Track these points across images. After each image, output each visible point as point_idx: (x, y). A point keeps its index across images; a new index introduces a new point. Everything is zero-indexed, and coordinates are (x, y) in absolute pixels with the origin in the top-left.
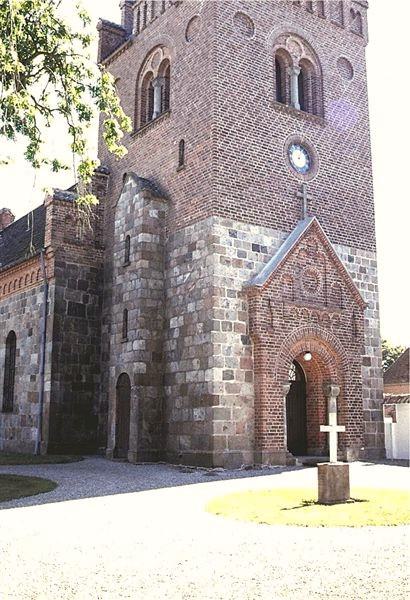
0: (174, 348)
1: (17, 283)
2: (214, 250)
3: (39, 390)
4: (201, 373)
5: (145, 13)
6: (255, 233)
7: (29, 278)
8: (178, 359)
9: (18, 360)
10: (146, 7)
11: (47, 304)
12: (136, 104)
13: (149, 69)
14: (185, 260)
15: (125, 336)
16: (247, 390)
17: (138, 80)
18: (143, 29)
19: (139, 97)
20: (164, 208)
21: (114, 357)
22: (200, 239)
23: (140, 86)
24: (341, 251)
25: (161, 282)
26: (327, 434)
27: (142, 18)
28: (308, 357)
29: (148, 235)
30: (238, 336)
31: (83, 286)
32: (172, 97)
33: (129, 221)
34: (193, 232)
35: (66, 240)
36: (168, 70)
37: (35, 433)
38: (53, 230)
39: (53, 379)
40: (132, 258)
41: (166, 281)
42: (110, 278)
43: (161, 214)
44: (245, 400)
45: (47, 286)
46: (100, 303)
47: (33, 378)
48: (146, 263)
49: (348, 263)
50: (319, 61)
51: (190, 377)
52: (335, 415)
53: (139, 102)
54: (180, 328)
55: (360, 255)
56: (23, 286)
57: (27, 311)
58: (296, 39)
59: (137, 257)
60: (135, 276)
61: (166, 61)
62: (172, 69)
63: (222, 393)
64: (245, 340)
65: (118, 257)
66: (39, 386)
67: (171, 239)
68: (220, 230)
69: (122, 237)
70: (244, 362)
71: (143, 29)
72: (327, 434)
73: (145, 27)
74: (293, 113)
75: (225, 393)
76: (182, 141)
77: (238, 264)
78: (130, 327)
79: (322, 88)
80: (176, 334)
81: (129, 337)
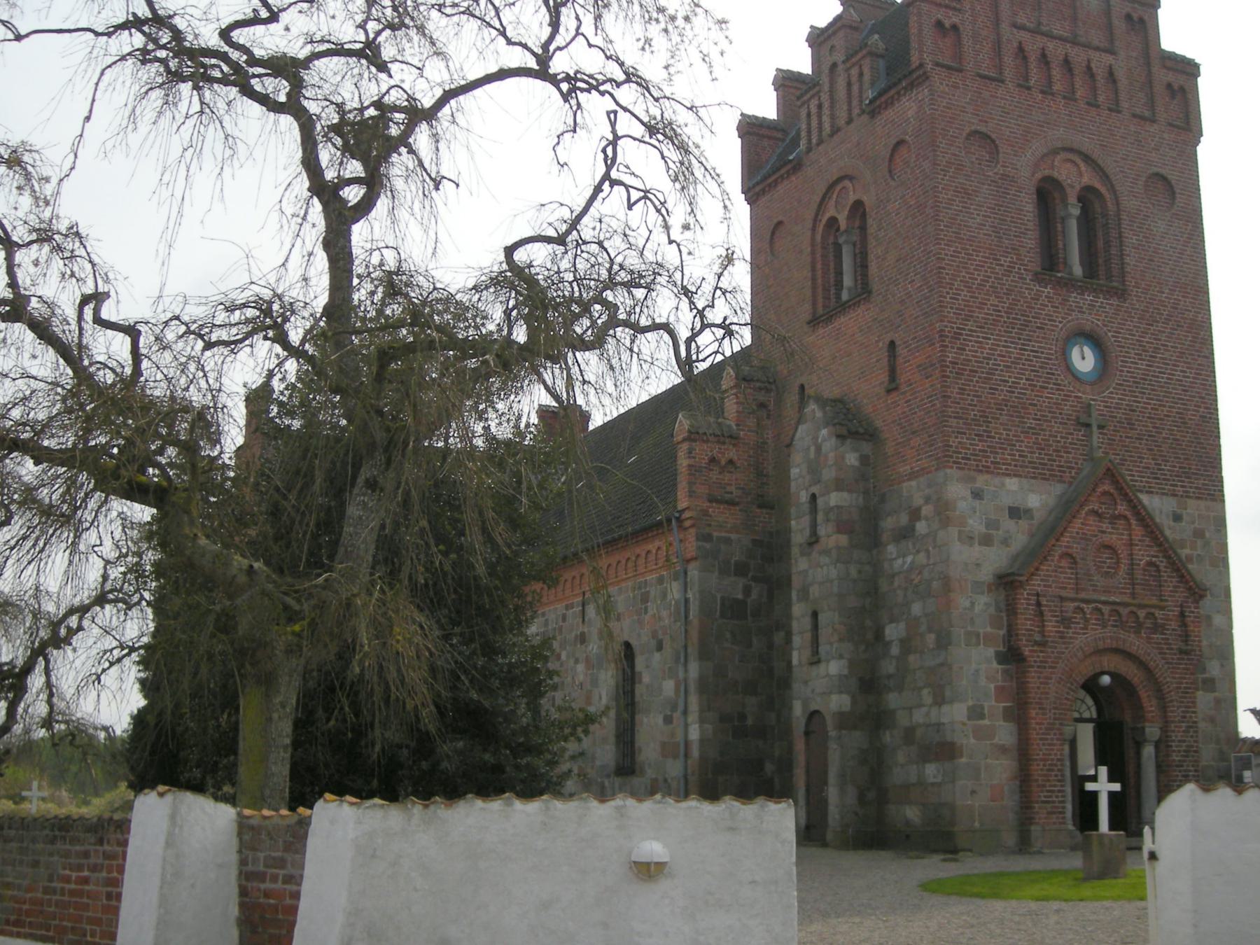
1: (630, 564)
2: (946, 522)
4: (934, 711)
5: (820, 116)
6: (1012, 488)
7: (652, 557)
8: (900, 688)
9: (639, 690)
10: (820, 106)
11: (687, 601)
12: (813, 269)
13: (831, 212)
14: (905, 534)
15: (816, 652)
16: (1005, 734)
17: (814, 229)
18: (818, 145)
19: (818, 256)
20: (867, 448)
21: (796, 686)
23: (819, 238)
24: (1157, 505)
26: (1095, 795)
27: (814, 123)
28: (1106, 680)
29: (845, 495)
30: (990, 652)
31: (741, 570)
32: (873, 269)
33: (814, 470)
34: (914, 491)
35: (712, 500)
36: (864, 215)
38: (691, 484)
39: (702, 721)
40: (822, 531)
43: (864, 460)
44: (1003, 750)
45: (686, 573)
47: (668, 720)
48: (843, 540)
49: (1172, 523)
50: (1112, 186)
51: (919, 717)
52: (830, 821)
53: (819, 266)
54: (902, 641)
55: (1193, 508)
56: (641, 569)
60: (827, 560)
61: (858, 205)
63: (968, 741)
64: (1002, 658)
65: (799, 528)
67: (883, 499)
68: (957, 491)
69: (804, 497)
70: (1000, 690)
71: (818, 145)
72: (1095, 795)
73: (820, 142)
74: (1069, 284)
75: (972, 741)
77: (986, 541)
78: (822, 640)
79: (1120, 233)
80: (895, 650)
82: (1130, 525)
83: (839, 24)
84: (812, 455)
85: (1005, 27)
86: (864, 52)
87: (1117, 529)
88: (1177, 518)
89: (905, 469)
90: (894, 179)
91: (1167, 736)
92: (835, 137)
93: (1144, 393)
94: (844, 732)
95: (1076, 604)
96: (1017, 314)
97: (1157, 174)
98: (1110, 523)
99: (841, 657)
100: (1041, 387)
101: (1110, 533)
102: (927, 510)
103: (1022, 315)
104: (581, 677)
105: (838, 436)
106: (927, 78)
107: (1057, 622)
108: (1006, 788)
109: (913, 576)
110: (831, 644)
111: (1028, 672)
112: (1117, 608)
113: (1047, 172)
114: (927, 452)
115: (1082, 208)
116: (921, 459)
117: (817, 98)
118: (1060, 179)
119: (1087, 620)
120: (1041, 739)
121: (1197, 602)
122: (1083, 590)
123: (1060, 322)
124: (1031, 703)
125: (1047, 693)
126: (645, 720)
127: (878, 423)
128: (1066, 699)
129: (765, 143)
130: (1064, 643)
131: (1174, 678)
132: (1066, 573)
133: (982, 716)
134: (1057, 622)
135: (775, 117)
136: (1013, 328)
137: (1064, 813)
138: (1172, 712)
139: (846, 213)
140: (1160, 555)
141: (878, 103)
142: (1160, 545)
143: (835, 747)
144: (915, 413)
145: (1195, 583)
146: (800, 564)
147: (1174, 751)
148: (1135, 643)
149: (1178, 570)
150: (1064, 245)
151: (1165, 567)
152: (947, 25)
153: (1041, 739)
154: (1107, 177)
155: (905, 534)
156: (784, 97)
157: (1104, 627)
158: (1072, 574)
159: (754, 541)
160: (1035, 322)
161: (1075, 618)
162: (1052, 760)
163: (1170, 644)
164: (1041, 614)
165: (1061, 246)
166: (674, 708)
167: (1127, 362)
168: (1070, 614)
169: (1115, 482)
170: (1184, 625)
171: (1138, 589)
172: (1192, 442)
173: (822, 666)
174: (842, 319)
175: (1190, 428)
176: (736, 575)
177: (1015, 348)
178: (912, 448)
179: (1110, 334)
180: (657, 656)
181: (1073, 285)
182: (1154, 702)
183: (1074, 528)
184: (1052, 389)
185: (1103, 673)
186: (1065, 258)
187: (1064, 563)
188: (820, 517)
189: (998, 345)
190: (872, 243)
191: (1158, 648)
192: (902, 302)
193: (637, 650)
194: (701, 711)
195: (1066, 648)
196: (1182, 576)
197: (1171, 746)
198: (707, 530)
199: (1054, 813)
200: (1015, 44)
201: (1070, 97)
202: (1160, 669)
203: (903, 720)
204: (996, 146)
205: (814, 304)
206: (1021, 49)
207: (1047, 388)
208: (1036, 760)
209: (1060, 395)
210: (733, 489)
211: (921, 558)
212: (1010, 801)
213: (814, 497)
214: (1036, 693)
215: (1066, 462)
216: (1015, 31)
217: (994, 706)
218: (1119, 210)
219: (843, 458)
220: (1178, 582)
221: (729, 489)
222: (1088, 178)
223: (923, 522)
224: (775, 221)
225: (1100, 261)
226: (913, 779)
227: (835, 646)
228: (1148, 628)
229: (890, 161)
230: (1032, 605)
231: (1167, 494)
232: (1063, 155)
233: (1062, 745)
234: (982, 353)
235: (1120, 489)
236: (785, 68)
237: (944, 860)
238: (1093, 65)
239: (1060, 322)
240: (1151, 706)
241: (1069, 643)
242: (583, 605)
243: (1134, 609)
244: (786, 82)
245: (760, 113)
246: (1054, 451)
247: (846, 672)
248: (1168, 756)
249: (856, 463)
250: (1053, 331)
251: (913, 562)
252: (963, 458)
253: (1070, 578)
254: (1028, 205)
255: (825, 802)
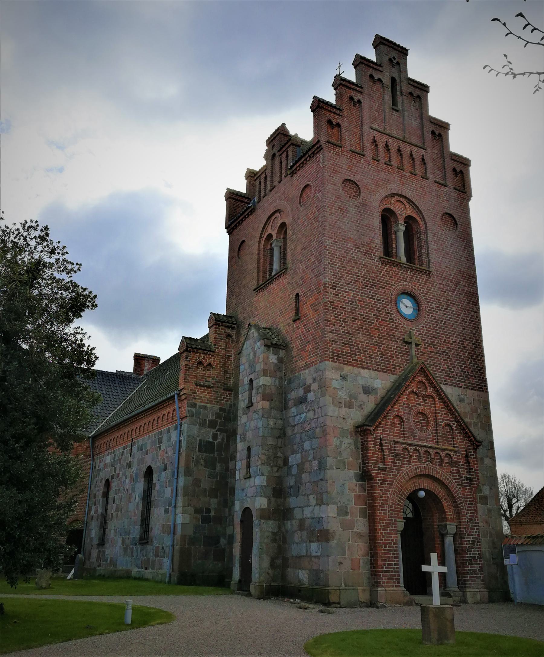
0: (292, 483)
1: (155, 422)
3: (171, 523)
4: (317, 508)
7: (165, 418)
9: (154, 493)
10: (266, 178)
17: (260, 242)
19: (261, 256)
20: (282, 353)
22: (314, 382)
23: (262, 246)
25: (280, 422)
26: (429, 574)
28: (422, 494)
29: (268, 378)
30: (351, 473)
31: (212, 424)
32: (289, 257)
33: (252, 366)
34: (307, 375)
36: (285, 233)
37: (167, 562)
39: (184, 512)
40: (254, 399)
41: (285, 420)
42: (236, 418)
43: (280, 360)
44: (359, 535)
46: (228, 441)
47: (167, 511)
48: (266, 404)
51: (307, 512)
53: (261, 261)
54: (298, 465)
56: (160, 425)
57: (163, 447)
58: (401, 199)
59: (259, 399)
61: (283, 225)
62: (288, 231)
65: (243, 401)
66: (172, 518)
67: (290, 382)
69: (246, 381)
70: (357, 497)
71: (264, 197)
72: (429, 574)
74: (399, 265)
76: (297, 295)
77: (350, 406)
80: (294, 471)
81: (252, 473)
82: (435, 401)
83: (277, 133)
84: (251, 357)
85: (366, 128)
86: (289, 143)
87: (428, 403)
88: (462, 400)
89: (301, 364)
90: (302, 206)
91: (461, 531)
92: (273, 191)
93: (441, 328)
94: (262, 521)
95: (404, 446)
96: (369, 279)
97: (445, 213)
98: (423, 399)
99: (262, 474)
100: (382, 320)
101: (423, 405)
102: (314, 386)
103: (372, 280)
104: (127, 487)
105: (265, 346)
106: (322, 148)
107: (393, 456)
108: (362, 561)
109: (306, 426)
110: (257, 466)
111: (375, 486)
112: (428, 450)
113: (387, 206)
114: (315, 353)
115: (406, 226)
116: (312, 357)
117: (264, 173)
118: (394, 210)
119: (410, 456)
120: (383, 530)
121: (476, 449)
122: (408, 437)
123: (394, 285)
124: (377, 506)
125: (387, 500)
126: (155, 511)
127: (288, 339)
128: (398, 504)
129: (239, 203)
130: (396, 470)
131: (464, 495)
132: (397, 427)
133: (346, 514)
134: (393, 456)
135: (245, 192)
136: (367, 286)
137: (398, 579)
138: (463, 516)
139: (277, 230)
140: (453, 420)
141: (295, 167)
142: (453, 414)
143: (257, 530)
144: (309, 331)
145: (474, 437)
146: (243, 419)
147: (466, 541)
148: (440, 472)
149: (464, 429)
150: (396, 246)
151: (456, 427)
152: (334, 123)
153: (383, 530)
154: (420, 211)
155: (302, 400)
156: (250, 182)
157: (421, 461)
158: (401, 428)
159: (221, 409)
160: (379, 284)
161: (404, 454)
162: (391, 543)
163: (460, 473)
164: (383, 451)
165: (394, 246)
166: (170, 505)
167: (431, 310)
168: (400, 452)
169: (426, 376)
170: (468, 462)
171: (441, 439)
172: (469, 358)
173: (252, 479)
174: (272, 286)
175: (467, 350)
176: (208, 427)
177: (368, 297)
178: (306, 351)
179: (422, 294)
180: (164, 473)
181: (401, 266)
182: (452, 509)
183: (402, 401)
184: (388, 321)
185: (420, 489)
186: (397, 253)
187: (397, 421)
188: (254, 392)
189: (357, 295)
190: (288, 241)
191: (453, 476)
192: (304, 271)
193: (154, 471)
194: (184, 506)
195: (398, 473)
196: (466, 433)
197: (464, 538)
198: (194, 401)
199: (392, 579)
200: (372, 138)
201: (401, 168)
202: (455, 489)
203: (298, 514)
204: (359, 189)
205: (258, 280)
206: (374, 141)
207: (386, 321)
208: (380, 543)
209: (393, 325)
210: (210, 379)
211: (311, 415)
212: (364, 570)
213: (251, 380)
214: (380, 500)
215: (396, 363)
216: (372, 131)
217: (355, 507)
218: (426, 228)
219: (268, 358)
220: (463, 436)
221: (208, 379)
222: (410, 212)
223: (312, 393)
224: (241, 241)
225: (416, 257)
226: (304, 553)
227: (259, 467)
228: (447, 463)
229: (300, 197)
230: (377, 445)
231: (455, 386)
232: (397, 198)
233: (396, 534)
234: (349, 298)
235: (429, 380)
236: (252, 168)
237: (321, 611)
238: (413, 153)
239: (394, 285)
240: (450, 511)
241: (400, 470)
242: (131, 446)
243: (439, 451)
244: (251, 176)
245: (237, 189)
246: (390, 356)
247: (265, 483)
248: (461, 544)
249: (276, 361)
250: (390, 290)
251: (306, 417)
252: (335, 356)
253: (400, 430)
254: (377, 223)
255: (250, 565)
